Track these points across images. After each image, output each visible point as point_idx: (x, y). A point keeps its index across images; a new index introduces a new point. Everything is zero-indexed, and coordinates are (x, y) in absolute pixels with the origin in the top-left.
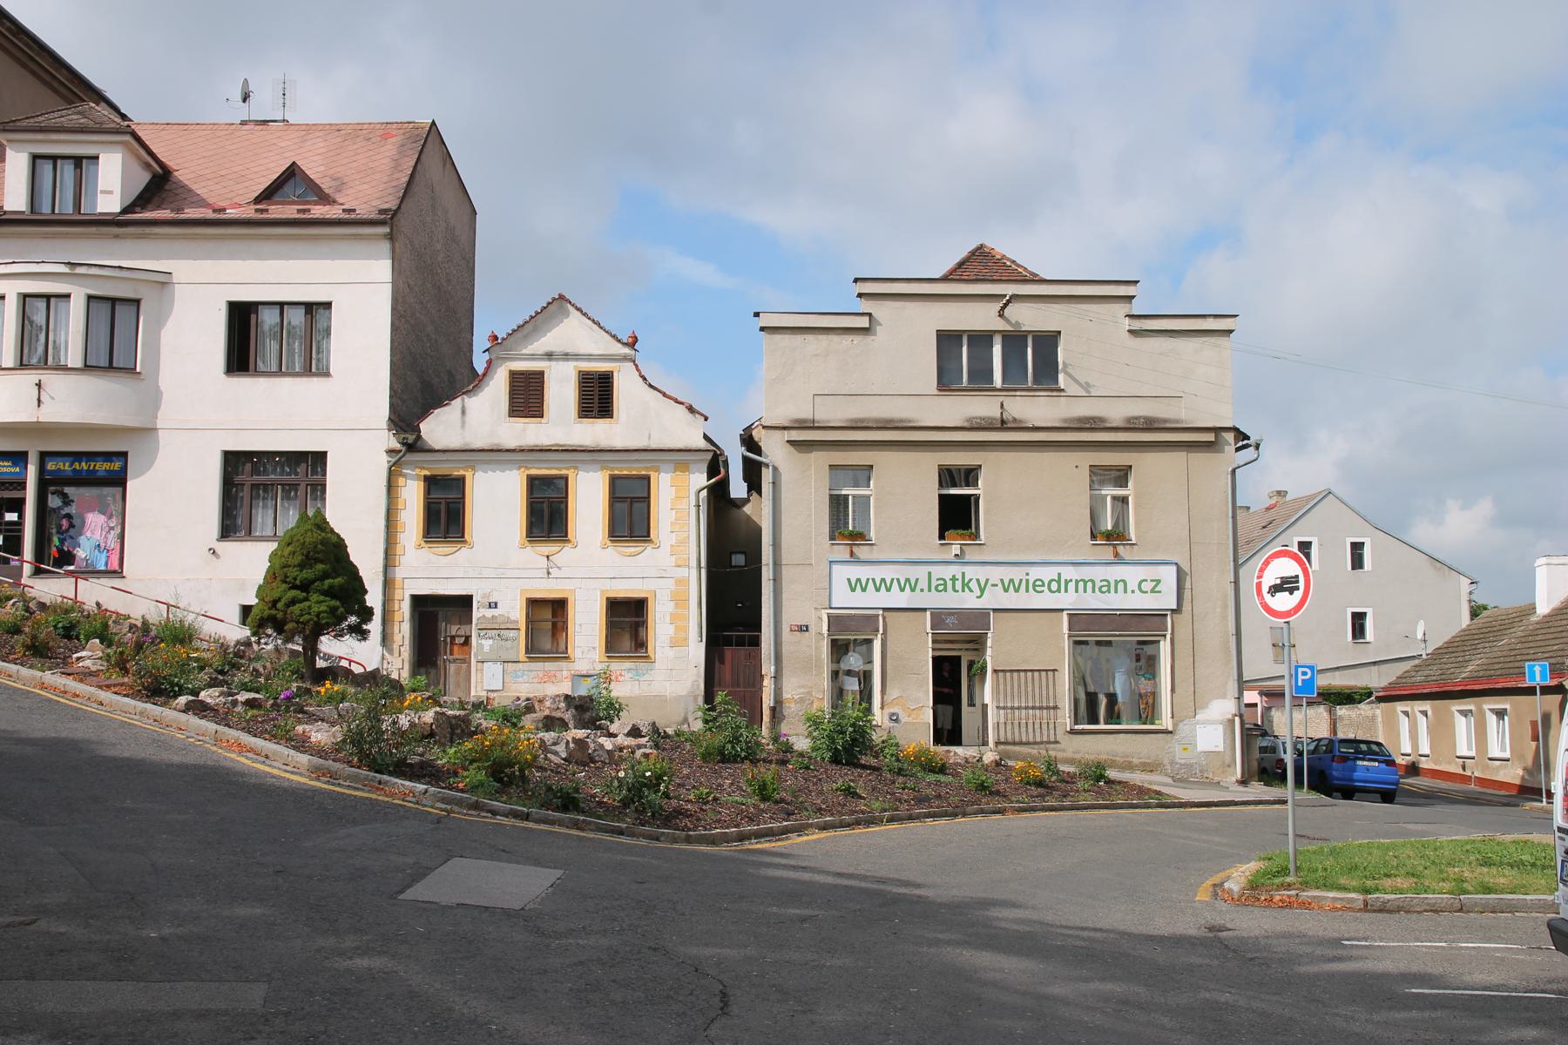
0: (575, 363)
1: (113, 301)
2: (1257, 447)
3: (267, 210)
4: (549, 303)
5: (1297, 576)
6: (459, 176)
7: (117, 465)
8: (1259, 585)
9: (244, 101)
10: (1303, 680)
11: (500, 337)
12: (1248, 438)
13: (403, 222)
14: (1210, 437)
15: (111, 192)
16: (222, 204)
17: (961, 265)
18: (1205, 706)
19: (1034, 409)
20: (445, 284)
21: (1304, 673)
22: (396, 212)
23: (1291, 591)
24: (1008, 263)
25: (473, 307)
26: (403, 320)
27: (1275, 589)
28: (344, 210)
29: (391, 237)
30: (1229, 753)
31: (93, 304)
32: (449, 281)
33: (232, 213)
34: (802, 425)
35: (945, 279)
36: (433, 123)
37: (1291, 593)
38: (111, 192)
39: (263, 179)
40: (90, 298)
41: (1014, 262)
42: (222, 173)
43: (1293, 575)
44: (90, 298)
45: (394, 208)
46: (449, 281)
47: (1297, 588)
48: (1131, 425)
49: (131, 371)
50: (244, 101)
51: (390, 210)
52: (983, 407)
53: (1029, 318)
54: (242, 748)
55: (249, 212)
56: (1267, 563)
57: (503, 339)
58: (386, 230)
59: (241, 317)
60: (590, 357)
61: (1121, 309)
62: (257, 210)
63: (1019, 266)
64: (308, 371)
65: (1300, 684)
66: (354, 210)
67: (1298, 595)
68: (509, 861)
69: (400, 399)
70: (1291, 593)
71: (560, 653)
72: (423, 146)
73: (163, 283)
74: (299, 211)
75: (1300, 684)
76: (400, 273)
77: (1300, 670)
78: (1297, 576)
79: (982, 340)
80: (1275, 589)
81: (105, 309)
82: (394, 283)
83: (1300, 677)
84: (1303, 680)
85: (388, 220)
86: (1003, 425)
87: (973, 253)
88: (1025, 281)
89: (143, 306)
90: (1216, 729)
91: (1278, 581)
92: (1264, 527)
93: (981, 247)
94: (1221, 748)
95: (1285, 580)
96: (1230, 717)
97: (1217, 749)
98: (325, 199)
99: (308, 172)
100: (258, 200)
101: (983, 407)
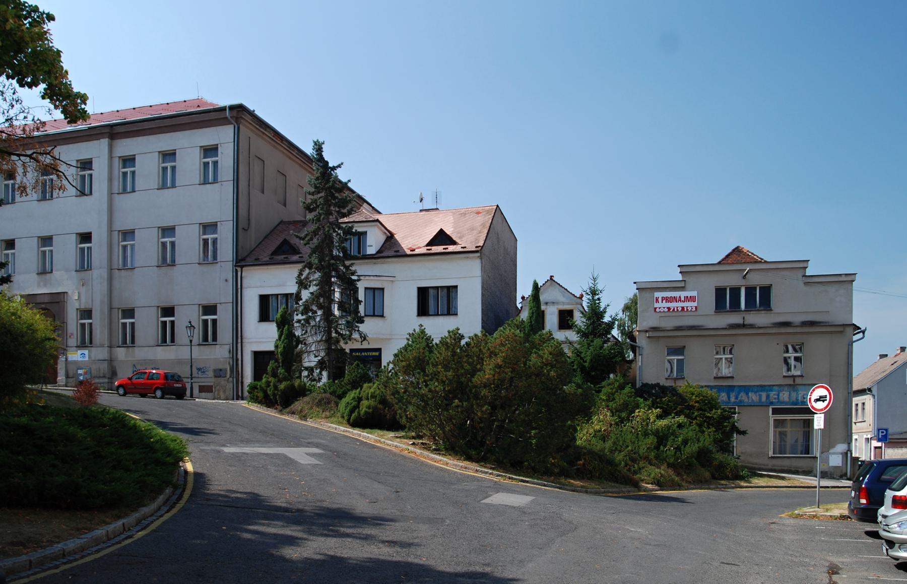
0: (557, 307)
1: (374, 289)
2: (863, 332)
3: (431, 249)
4: (546, 282)
5: (826, 396)
6: (510, 227)
7: (377, 354)
8: (810, 399)
9: (421, 201)
10: (882, 435)
11: (526, 297)
12: (860, 329)
13: (485, 250)
14: (841, 329)
15: (372, 246)
16: (414, 247)
17: (727, 256)
18: (833, 447)
19: (759, 318)
20: (504, 273)
21: (882, 432)
22: (482, 247)
23: (823, 401)
24: (750, 254)
25: (516, 281)
26: (486, 291)
27: (817, 400)
28: (462, 248)
29: (481, 258)
30: (844, 466)
31: (367, 291)
32: (505, 272)
33: (417, 251)
34: (655, 329)
35: (720, 263)
36: (498, 206)
37: (823, 402)
38: (372, 246)
39: (430, 235)
40: (366, 288)
41: (752, 254)
42: (413, 234)
43: (825, 395)
44: (366, 288)
45: (482, 245)
46: (505, 272)
47: (826, 400)
48: (805, 324)
49: (382, 316)
50: (421, 201)
51: (480, 246)
52: (735, 319)
53: (757, 280)
54: (428, 458)
55: (424, 250)
56: (814, 390)
57: (527, 298)
58: (478, 254)
59: (423, 293)
60: (563, 303)
61: (800, 274)
62: (427, 250)
63: (755, 255)
64: (449, 313)
65: (880, 437)
66: (465, 247)
67: (826, 403)
68: (518, 494)
69: (486, 324)
70: (823, 402)
71: (801, 419)
72: (493, 217)
73: (392, 281)
74: (444, 249)
75: (880, 437)
76: (485, 272)
77: (880, 431)
78: (826, 396)
79: (735, 291)
80: (817, 400)
81: (371, 293)
82: (482, 276)
83: (880, 434)
84: (882, 435)
85: (479, 251)
86: (744, 326)
87: (734, 250)
88: (756, 262)
89: (385, 290)
90: (838, 457)
91: (818, 397)
92: (892, 364)
93: (738, 247)
94: (841, 465)
95: (821, 397)
96: (845, 451)
97: (838, 465)
98: (454, 243)
99: (446, 232)
100: (428, 245)
101: (735, 319)
